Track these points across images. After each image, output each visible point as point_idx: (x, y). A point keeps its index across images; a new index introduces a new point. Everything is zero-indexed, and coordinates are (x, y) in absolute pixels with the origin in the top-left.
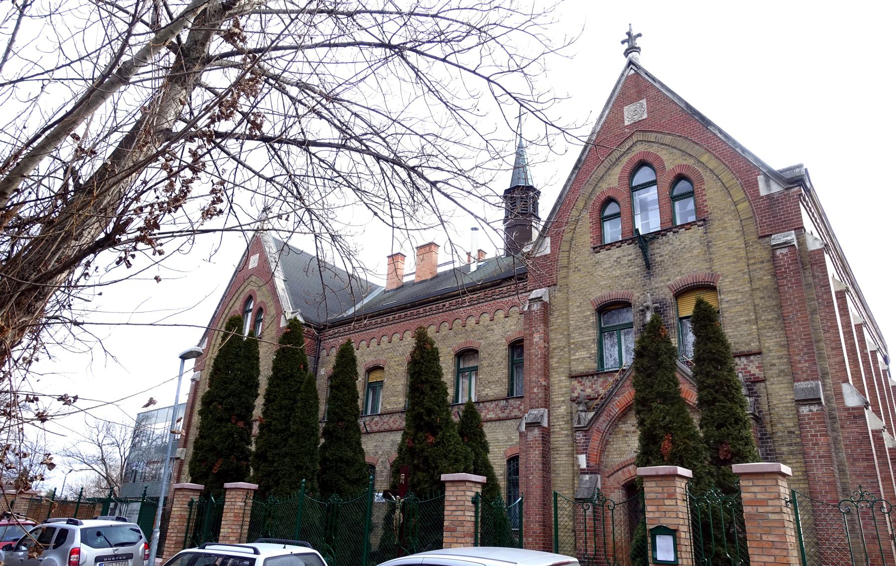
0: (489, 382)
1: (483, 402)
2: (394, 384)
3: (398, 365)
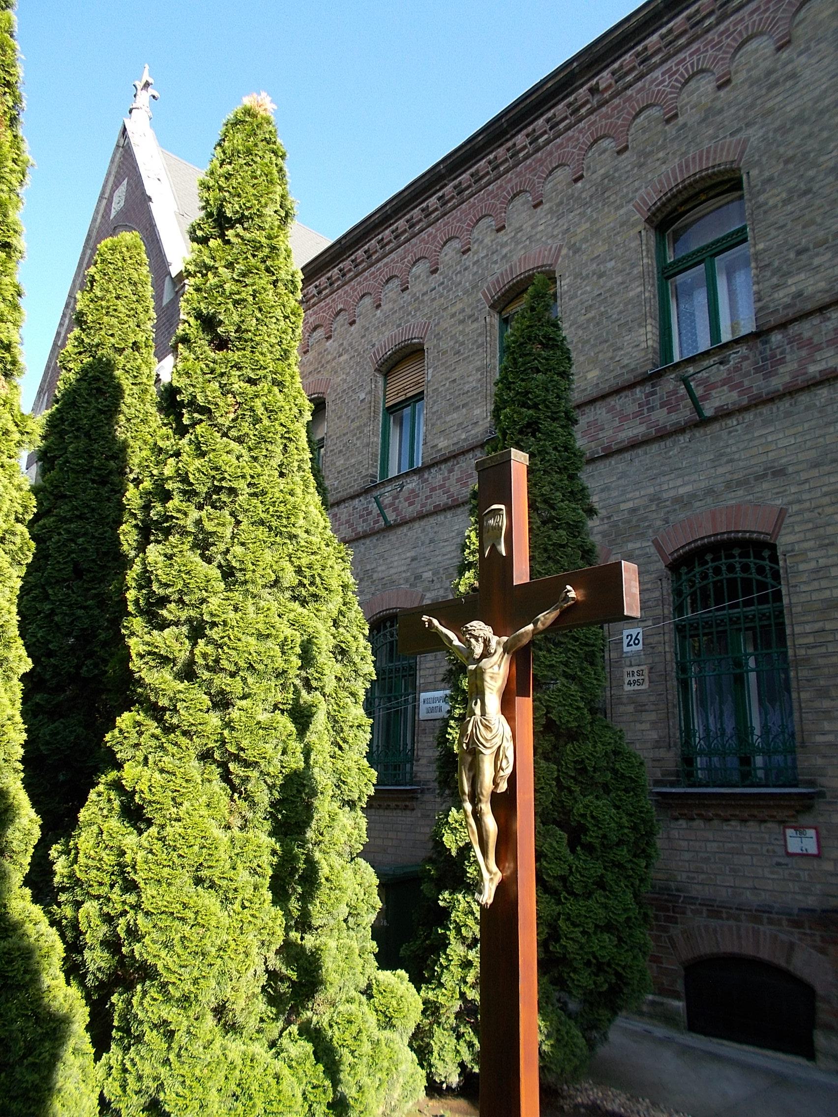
0: (799, 253)
1: (783, 326)
2: (456, 375)
3: (462, 322)
